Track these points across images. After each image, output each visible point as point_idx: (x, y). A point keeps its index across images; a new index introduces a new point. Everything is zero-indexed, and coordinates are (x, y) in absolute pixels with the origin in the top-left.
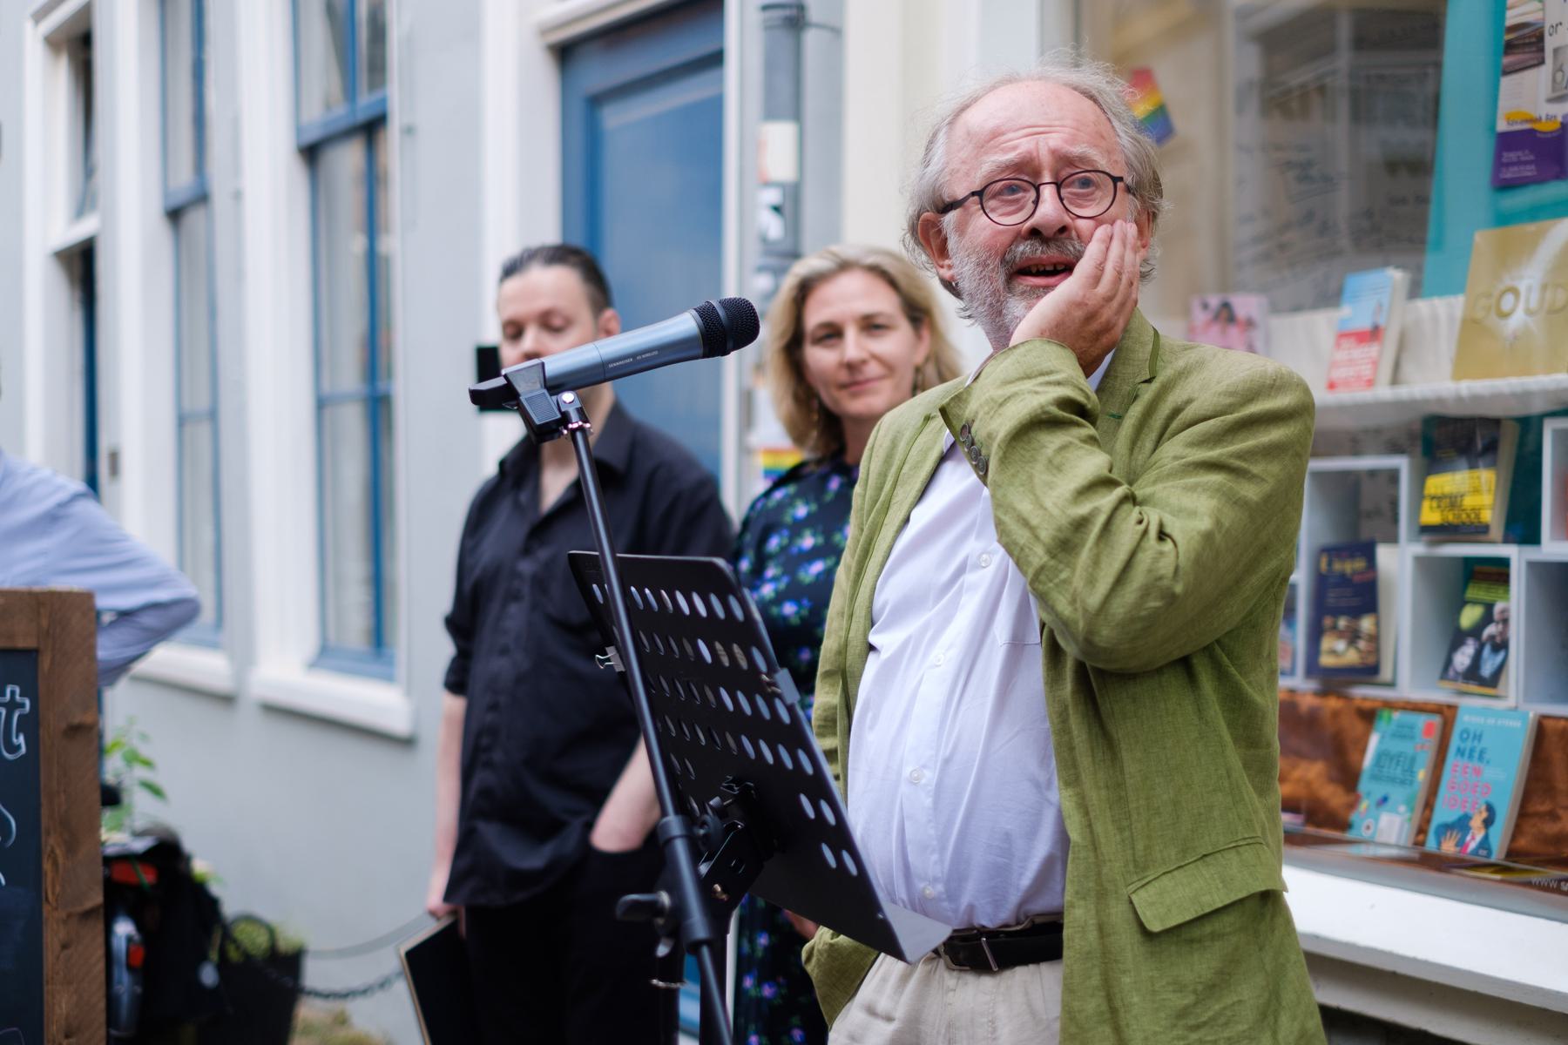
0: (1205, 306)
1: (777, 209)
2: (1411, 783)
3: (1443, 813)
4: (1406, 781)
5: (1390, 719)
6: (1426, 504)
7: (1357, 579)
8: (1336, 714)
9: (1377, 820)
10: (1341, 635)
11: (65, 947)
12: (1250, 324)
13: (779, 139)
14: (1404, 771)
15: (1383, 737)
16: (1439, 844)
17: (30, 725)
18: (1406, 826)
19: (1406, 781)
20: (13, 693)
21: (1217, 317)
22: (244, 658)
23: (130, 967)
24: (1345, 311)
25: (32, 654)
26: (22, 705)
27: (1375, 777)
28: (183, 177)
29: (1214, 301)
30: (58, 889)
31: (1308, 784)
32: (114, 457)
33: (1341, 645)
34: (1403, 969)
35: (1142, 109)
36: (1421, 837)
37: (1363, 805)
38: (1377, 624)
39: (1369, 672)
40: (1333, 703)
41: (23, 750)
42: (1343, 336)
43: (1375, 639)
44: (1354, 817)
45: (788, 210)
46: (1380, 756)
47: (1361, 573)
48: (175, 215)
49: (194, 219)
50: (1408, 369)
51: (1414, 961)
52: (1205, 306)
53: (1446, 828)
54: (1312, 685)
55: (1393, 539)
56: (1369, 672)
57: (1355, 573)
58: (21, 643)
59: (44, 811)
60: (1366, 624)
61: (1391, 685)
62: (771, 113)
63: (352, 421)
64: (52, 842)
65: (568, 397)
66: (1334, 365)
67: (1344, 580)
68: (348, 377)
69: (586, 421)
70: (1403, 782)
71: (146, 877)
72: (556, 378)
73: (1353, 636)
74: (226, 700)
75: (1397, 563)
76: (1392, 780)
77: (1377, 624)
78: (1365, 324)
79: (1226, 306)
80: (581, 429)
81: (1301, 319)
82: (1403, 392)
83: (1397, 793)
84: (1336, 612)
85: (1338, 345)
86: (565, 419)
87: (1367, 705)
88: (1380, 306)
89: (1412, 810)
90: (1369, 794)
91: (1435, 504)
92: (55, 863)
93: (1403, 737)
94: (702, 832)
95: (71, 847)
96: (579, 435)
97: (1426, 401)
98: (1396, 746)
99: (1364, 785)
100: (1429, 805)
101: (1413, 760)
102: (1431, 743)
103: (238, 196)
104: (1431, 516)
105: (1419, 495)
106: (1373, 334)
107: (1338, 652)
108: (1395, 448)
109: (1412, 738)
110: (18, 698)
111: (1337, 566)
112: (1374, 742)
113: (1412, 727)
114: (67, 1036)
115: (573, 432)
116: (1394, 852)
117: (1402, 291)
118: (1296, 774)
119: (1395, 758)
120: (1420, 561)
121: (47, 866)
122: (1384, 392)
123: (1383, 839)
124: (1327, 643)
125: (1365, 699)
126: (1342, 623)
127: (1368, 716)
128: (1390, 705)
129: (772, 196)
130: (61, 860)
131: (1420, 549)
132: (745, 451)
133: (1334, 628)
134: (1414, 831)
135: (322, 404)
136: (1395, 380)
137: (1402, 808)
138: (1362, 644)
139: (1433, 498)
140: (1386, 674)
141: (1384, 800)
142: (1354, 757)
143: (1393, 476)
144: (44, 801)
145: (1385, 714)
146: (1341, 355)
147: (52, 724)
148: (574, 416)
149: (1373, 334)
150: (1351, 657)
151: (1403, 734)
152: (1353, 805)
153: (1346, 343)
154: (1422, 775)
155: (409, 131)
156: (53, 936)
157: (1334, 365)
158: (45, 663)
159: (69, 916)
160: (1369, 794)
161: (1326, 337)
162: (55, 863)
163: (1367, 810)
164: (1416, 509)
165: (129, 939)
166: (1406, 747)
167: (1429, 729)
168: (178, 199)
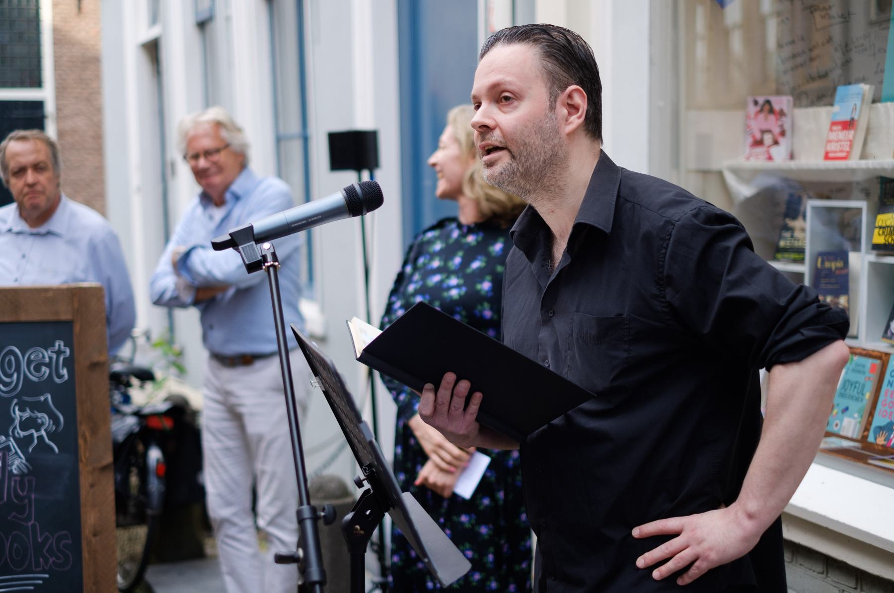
0: (756, 103)
2: (862, 400)
3: (879, 420)
6: (876, 231)
9: (842, 421)
11: (92, 486)
12: (782, 113)
16: (876, 439)
17: (69, 363)
18: (858, 425)
20: (59, 345)
24: (836, 108)
25: (69, 324)
26: (65, 352)
27: (842, 395)
29: (761, 100)
30: (87, 455)
34: (831, 527)
36: (866, 433)
41: (66, 377)
42: (834, 124)
46: (846, 382)
47: (841, 269)
48: (202, 25)
49: (209, 28)
50: (872, 147)
51: (837, 522)
52: (756, 103)
53: (881, 428)
57: (837, 269)
58: (64, 317)
59: (79, 411)
61: (855, 337)
64: (83, 429)
65: (266, 245)
66: (829, 141)
67: (830, 273)
68: (294, 127)
70: (857, 399)
71: (167, 424)
72: (261, 233)
75: (860, 262)
76: (852, 397)
77: (848, 301)
78: (846, 117)
79: (768, 102)
80: (272, 266)
81: (811, 111)
82: (869, 164)
83: (854, 406)
85: (831, 130)
86: (264, 258)
89: (862, 416)
91: (881, 232)
93: (859, 372)
94: (322, 514)
95: (94, 431)
96: (271, 269)
97: (875, 170)
98: (854, 377)
100: (871, 414)
101: (864, 386)
102: (874, 377)
103: (228, 19)
104: (879, 239)
105: (872, 227)
106: (848, 125)
109: (864, 373)
110: (62, 347)
111: (827, 265)
113: (864, 366)
114: (95, 535)
115: (268, 267)
116: (846, 444)
119: (853, 384)
120: (874, 266)
121: (81, 442)
122: (854, 162)
123: (842, 433)
130: (88, 438)
131: (872, 257)
135: (279, 140)
136: (863, 156)
137: (856, 415)
139: (880, 227)
141: (846, 409)
143: (859, 210)
144: (78, 405)
146: (833, 136)
148: (269, 258)
149: (848, 125)
151: (858, 370)
154: (868, 395)
156: (85, 481)
157: (829, 141)
158: (77, 328)
159: (94, 469)
161: (825, 123)
163: (837, 413)
164: (870, 235)
165: (158, 461)
166: (860, 378)
167: (873, 369)
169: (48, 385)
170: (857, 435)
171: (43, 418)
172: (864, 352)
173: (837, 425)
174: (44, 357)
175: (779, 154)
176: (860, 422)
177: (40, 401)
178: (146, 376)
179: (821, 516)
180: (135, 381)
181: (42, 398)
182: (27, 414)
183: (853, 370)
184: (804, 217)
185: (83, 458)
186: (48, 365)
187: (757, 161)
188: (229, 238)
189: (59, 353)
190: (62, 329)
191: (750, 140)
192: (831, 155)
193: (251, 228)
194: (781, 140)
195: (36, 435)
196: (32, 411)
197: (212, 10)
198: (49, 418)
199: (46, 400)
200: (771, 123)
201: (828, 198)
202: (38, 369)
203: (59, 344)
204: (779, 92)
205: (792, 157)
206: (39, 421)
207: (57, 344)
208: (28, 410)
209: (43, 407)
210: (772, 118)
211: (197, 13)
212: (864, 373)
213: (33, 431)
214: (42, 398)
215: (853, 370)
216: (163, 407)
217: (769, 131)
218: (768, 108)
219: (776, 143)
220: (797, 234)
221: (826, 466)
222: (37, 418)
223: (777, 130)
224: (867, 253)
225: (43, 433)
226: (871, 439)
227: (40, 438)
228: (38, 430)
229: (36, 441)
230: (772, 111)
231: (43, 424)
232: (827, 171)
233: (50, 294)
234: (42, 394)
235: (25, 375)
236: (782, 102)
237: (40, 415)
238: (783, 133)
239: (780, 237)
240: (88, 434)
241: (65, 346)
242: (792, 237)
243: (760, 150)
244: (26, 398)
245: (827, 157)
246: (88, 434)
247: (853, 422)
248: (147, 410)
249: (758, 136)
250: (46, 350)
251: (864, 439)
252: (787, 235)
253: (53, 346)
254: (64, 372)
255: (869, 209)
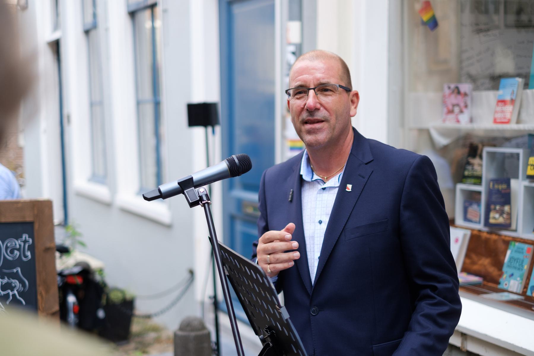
0: (449, 88)
1: (294, 53)
2: (522, 270)
4: (520, 269)
5: (515, 245)
6: (529, 167)
7: (503, 191)
8: (495, 241)
9: (509, 282)
10: (497, 212)
12: (466, 95)
13: (294, 27)
14: (519, 265)
15: (512, 252)
16: (532, 293)
17: (32, 248)
18: (520, 285)
19: (520, 269)
21: (453, 92)
22: (113, 190)
23: (74, 313)
24: (501, 92)
25: (31, 224)
27: (509, 266)
28: (89, 19)
29: (453, 86)
30: (43, 305)
31: (485, 266)
32: (69, 117)
33: (497, 216)
35: (426, 17)
36: (525, 290)
37: (505, 276)
38: (511, 209)
39: (507, 226)
40: (494, 237)
41: (30, 257)
43: (509, 214)
44: (501, 280)
45: (297, 53)
46: (511, 258)
47: (505, 190)
48: (87, 32)
49: (92, 33)
50: (524, 116)
51: (521, 348)
52: (449, 88)
54: (486, 229)
55: (516, 177)
56: (507, 226)
57: (502, 189)
58: (29, 219)
60: (507, 208)
61: (515, 231)
62: (291, 18)
63: (149, 109)
64: (41, 289)
66: (496, 112)
67: (498, 191)
68: (147, 94)
69: (209, 200)
70: (519, 269)
71: (78, 281)
73: (502, 213)
74: (108, 205)
75: (518, 186)
79: (457, 88)
82: (521, 127)
83: (517, 273)
84: (495, 204)
85: (497, 105)
87: (507, 239)
88: (513, 91)
89: (522, 280)
90: (506, 272)
91: (532, 168)
92: (42, 296)
93: (519, 252)
96: (206, 205)
98: (517, 256)
99: (505, 269)
100: (528, 278)
101: (523, 261)
103: (107, 30)
105: (526, 164)
107: (496, 218)
108: (518, 146)
109: (523, 253)
112: (509, 253)
113: (522, 249)
115: (204, 204)
117: (522, 86)
118: (481, 262)
120: (526, 188)
121: (39, 297)
122: (513, 126)
123: (510, 289)
124: (492, 215)
125: (506, 236)
126: (498, 207)
127: (507, 243)
128: (515, 240)
129: (292, 49)
131: (527, 183)
132: (283, 137)
133: (495, 209)
134: (523, 287)
135: (139, 103)
136: (518, 122)
137: (519, 279)
138: (505, 216)
139: (532, 165)
140: (513, 227)
142: (502, 258)
143: (518, 155)
145: (513, 243)
147: (39, 249)
148: (205, 198)
150: (501, 220)
152: (501, 275)
153: (500, 104)
155: (165, 11)
158: (36, 226)
160: (506, 272)
162: (42, 296)
163: (506, 278)
164: (525, 169)
165: (74, 304)
166: (521, 256)
168: (88, 27)
169: (18, 262)
170: (520, 291)
171: (16, 283)
172: (522, 241)
173: (506, 285)
174: (16, 245)
175: (464, 119)
176: (521, 283)
177: (13, 272)
178: (64, 251)
179: (510, 344)
180: (57, 254)
181: (15, 271)
182: (6, 280)
183: (516, 251)
184: (481, 157)
185: (41, 308)
186: (19, 250)
187: (450, 124)
188: (178, 186)
189: (25, 242)
190: (27, 227)
191: (445, 110)
192: (498, 120)
193: (192, 178)
194: (465, 111)
195: (11, 293)
196: (8, 279)
197: (27, 3)
198: (20, 283)
199: (17, 271)
200: (459, 100)
201: (494, 146)
202: (12, 252)
203: (25, 236)
204: (459, 81)
205: (471, 120)
206: (13, 285)
207: (24, 237)
208: (6, 278)
209: (15, 276)
210: (460, 97)
211: (84, 25)
212: (523, 253)
213: (9, 291)
214: (15, 271)
215: (516, 251)
216: (77, 270)
217: (458, 105)
218: (458, 91)
219: (461, 112)
220: (476, 167)
221: (505, 311)
222: (12, 283)
223: (462, 105)
224: (523, 180)
225: (16, 292)
226: (529, 293)
227: (14, 295)
228: (12, 290)
229: (11, 298)
230: (459, 93)
231: (15, 286)
232: (499, 131)
233: (20, 205)
234: (15, 268)
235: (4, 256)
236: (465, 87)
237: (13, 281)
238: (466, 106)
239: (465, 169)
240: (43, 293)
241: (29, 237)
242: (473, 169)
243: (451, 116)
244: (5, 271)
245: (495, 121)
246: (43, 293)
247: (517, 283)
248: (66, 272)
249: (450, 107)
250: (17, 240)
251: (524, 294)
252: (469, 168)
253: (21, 237)
254: (29, 254)
255: (524, 153)
